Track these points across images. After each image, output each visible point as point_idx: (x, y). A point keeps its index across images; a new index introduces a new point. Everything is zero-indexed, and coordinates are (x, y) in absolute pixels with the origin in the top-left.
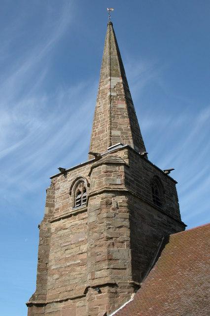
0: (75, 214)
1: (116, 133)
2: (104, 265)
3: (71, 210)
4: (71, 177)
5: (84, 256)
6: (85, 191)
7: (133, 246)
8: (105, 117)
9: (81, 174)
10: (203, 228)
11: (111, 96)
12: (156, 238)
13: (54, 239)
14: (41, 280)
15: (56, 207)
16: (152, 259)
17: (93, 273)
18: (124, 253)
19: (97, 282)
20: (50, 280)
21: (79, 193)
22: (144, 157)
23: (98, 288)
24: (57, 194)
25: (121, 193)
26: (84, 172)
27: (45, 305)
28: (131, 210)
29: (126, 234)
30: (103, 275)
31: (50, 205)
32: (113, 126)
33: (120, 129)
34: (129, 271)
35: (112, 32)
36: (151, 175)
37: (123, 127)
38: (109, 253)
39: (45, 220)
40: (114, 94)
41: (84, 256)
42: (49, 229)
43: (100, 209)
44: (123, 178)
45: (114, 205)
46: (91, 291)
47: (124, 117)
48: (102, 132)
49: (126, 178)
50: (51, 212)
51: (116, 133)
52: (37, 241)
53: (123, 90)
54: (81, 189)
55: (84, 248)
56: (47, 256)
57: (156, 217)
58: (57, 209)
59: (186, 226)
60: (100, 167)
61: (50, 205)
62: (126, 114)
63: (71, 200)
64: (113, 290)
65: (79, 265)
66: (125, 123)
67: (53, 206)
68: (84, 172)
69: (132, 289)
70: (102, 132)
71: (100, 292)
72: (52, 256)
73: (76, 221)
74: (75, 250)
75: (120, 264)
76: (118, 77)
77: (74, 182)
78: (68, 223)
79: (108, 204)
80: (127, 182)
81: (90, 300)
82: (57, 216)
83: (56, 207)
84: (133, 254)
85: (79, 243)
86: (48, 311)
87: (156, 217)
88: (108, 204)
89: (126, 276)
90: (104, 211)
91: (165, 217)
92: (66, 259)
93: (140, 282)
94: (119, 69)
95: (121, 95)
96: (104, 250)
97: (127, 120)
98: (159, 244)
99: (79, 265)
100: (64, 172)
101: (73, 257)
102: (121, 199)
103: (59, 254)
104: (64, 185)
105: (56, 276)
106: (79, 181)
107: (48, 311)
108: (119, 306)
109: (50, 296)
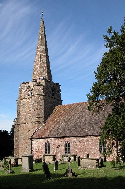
0: (28, 98)
1: (42, 70)
3: (27, 97)
4: (27, 85)
5: (31, 112)
8: (38, 63)
9: (30, 85)
11: (41, 54)
12: (52, 107)
13: (22, 105)
14: (19, 114)
15: (22, 94)
16: (50, 114)
18: (42, 113)
19: (34, 121)
21: (29, 91)
22: (51, 82)
23: (35, 122)
24: (23, 90)
26: (31, 85)
27: (19, 124)
28: (45, 100)
29: (43, 107)
30: (36, 119)
31: (20, 94)
32: (41, 67)
33: (43, 68)
34: (43, 118)
35: (43, 23)
36: (52, 86)
38: (38, 113)
39: (19, 99)
40: (42, 53)
41: (31, 112)
42: (20, 102)
43: (36, 100)
46: (33, 123)
47: (45, 63)
48: (37, 69)
49: (44, 90)
50: (20, 96)
51: (42, 70)
52: (16, 105)
53: (45, 52)
54: (30, 90)
56: (20, 110)
57: (52, 100)
58: (23, 95)
59: (60, 86)
61: (20, 94)
64: (39, 123)
65: (29, 114)
67: (21, 94)
68: (31, 85)
69: (44, 123)
70: (37, 69)
71: (35, 123)
72: (21, 110)
73: (28, 100)
74: (28, 109)
75: (41, 116)
76: (44, 46)
77: (28, 87)
78: (26, 100)
79: (38, 99)
80: (44, 92)
82: (23, 97)
83: (22, 94)
84: (45, 113)
86: (20, 126)
87: (52, 100)
88: (38, 99)
90: (37, 101)
92: (26, 112)
93: (46, 120)
94: (44, 42)
95: (44, 54)
96: (36, 112)
97: (46, 65)
98: (52, 109)
99: (29, 114)
100: (25, 83)
101: (28, 112)
102: (42, 97)
103: (23, 110)
104: (25, 87)
105: (23, 116)
106: (29, 87)
107: (21, 126)
108: (40, 127)
109: (21, 122)
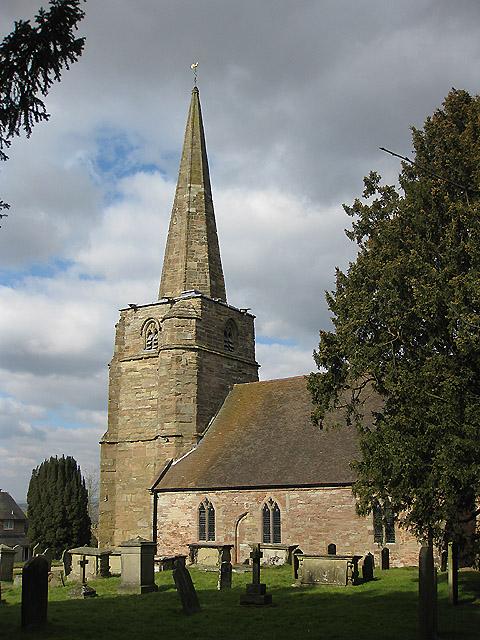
2: (173, 418)
4: (142, 315)
6: (156, 333)
7: (199, 401)
10: (17, 604)
17: (162, 424)
18: (191, 409)
20: (121, 421)
24: (128, 330)
25: (194, 350)
30: (171, 427)
34: (194, 424)
37: (200, 257)
40: (193, 210)
41: (155, 402)
44: (194, 333)
45: (184, 362)
50: (120, 350)
55: (155, 394)
56: (118, 397)
60: (179, 494)
62: (204, 239)
63: (141, 341)
66: (202, 253)
69: (196, 440)
80: (198, 337)
81: (160, 447)
82: (127, 355)
85: (149, 389)
88: (179, 360)
89: (192, 428)
91: (235, 363)
100: (134, 308)
102: (191, 356)
106: (150, 321)
